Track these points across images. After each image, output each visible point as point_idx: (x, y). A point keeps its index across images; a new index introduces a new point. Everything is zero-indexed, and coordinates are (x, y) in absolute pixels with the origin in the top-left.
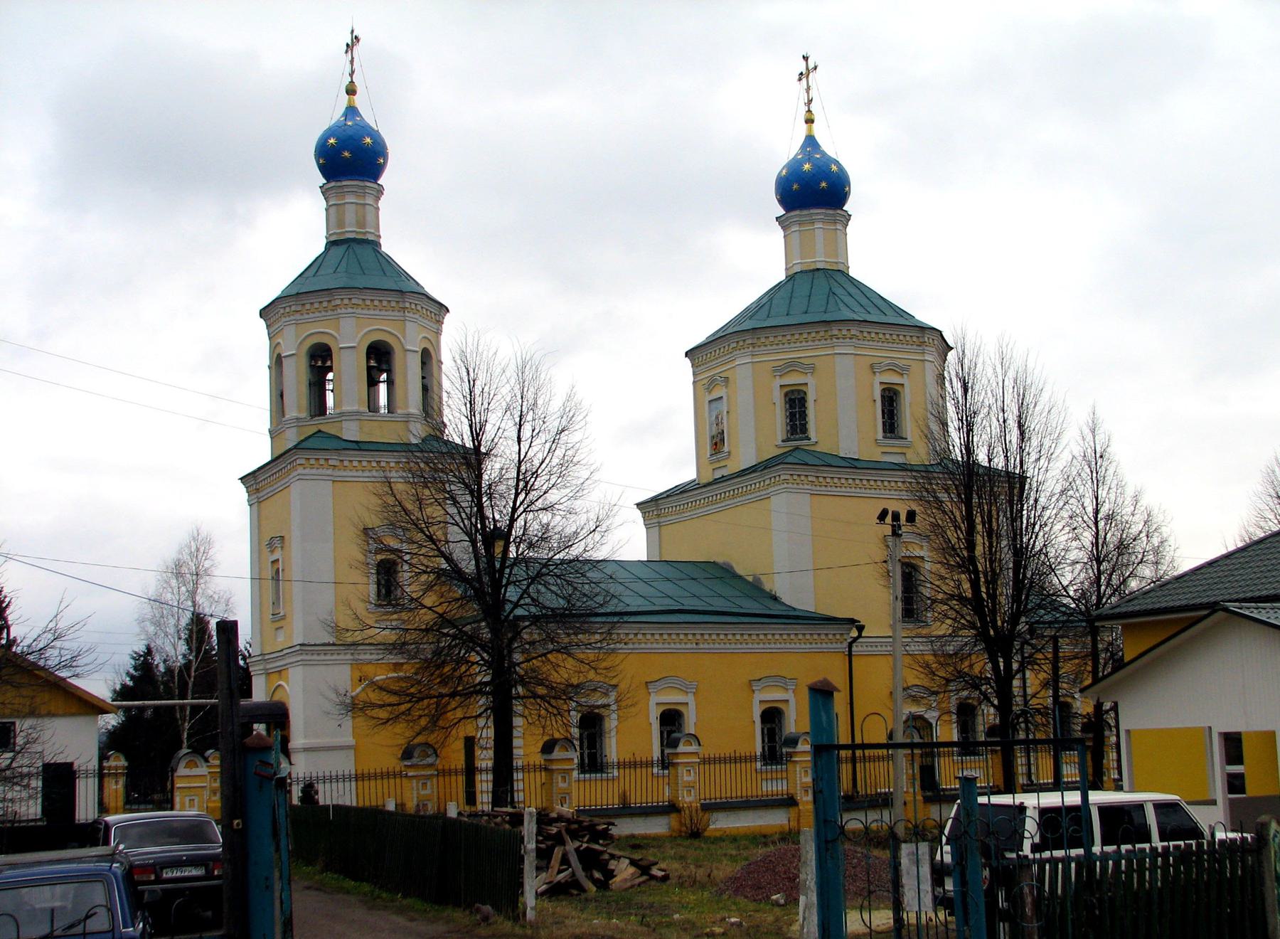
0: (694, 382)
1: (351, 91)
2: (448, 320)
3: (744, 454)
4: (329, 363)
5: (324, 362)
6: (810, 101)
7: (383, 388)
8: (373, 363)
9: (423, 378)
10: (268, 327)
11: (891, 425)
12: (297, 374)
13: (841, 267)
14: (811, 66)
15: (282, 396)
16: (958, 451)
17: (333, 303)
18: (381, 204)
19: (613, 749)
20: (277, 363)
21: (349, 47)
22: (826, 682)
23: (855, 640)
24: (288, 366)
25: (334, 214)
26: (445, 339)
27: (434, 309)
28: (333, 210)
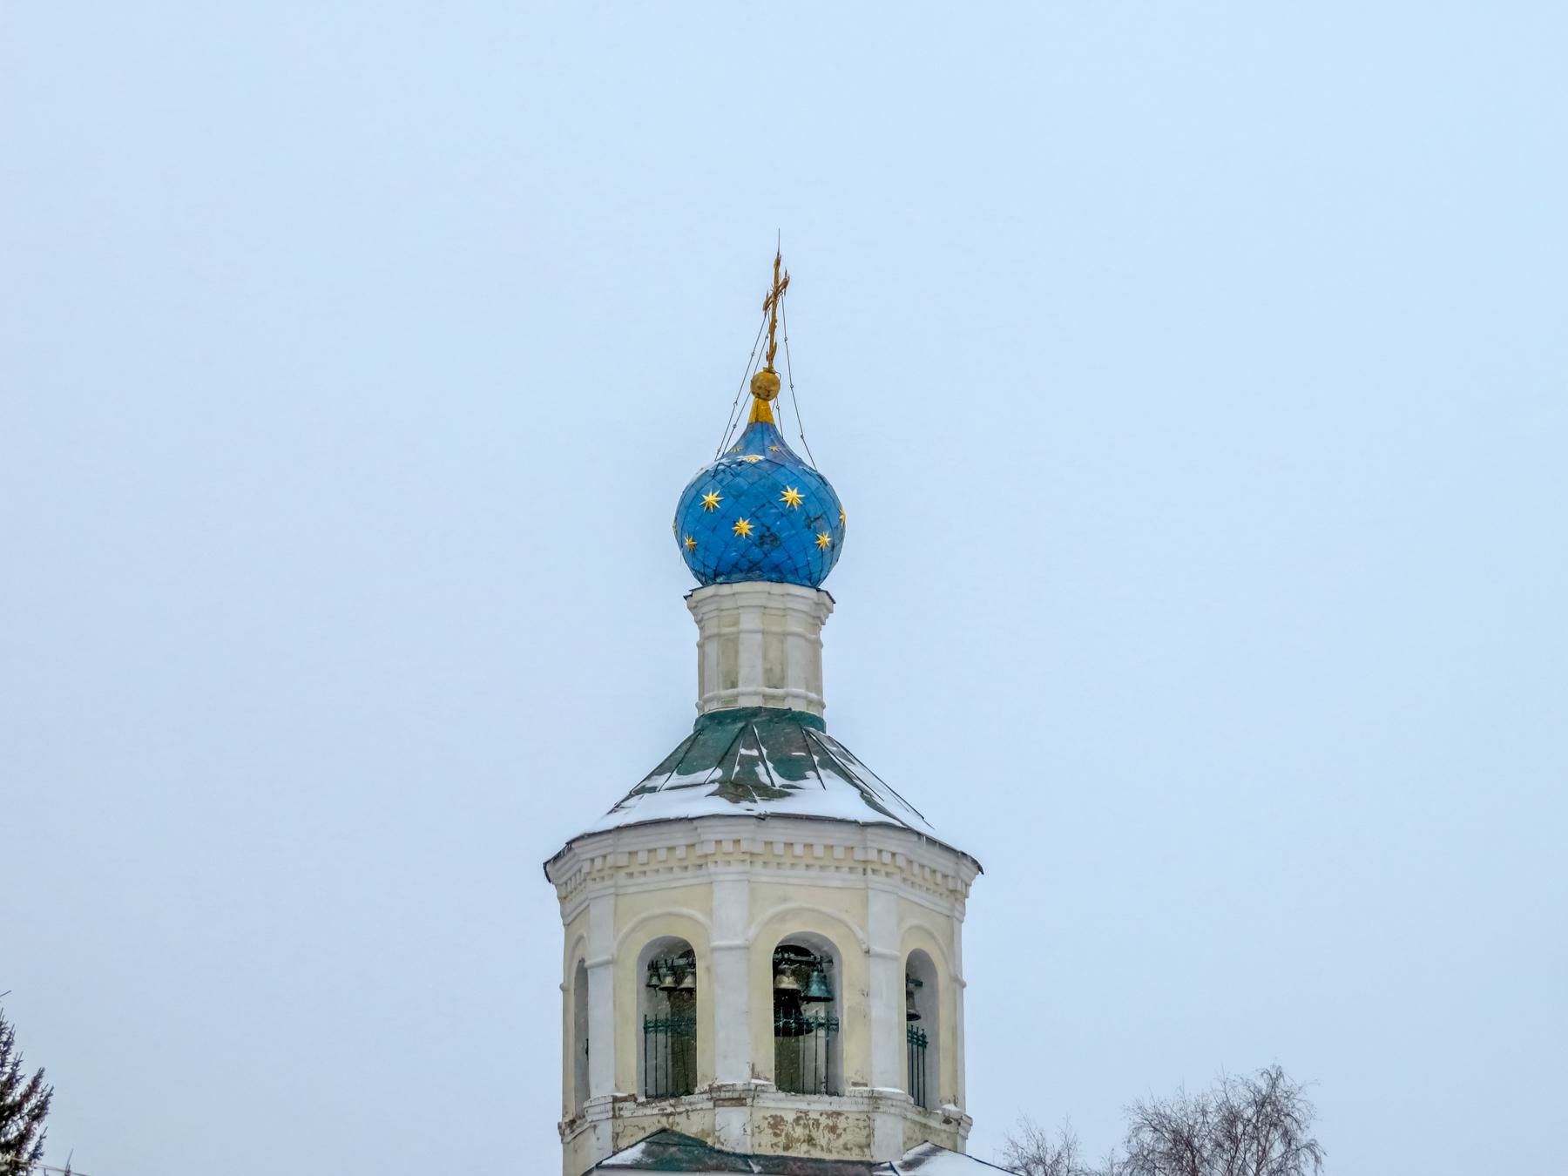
1: (765, 388)
2: (979, 887)
4: (688, 982)
9: (911, 1017)
10: (563, 899)
12: (621, 1007)
16: (772, 1104)
17: (699, 851)
18: (825, 634)
20: (579, 980)
21: (771, 303)
22: (822, 509)
25: (718, 648)
26: (970, 932)
27: (943, 862)
28: (712, 649)
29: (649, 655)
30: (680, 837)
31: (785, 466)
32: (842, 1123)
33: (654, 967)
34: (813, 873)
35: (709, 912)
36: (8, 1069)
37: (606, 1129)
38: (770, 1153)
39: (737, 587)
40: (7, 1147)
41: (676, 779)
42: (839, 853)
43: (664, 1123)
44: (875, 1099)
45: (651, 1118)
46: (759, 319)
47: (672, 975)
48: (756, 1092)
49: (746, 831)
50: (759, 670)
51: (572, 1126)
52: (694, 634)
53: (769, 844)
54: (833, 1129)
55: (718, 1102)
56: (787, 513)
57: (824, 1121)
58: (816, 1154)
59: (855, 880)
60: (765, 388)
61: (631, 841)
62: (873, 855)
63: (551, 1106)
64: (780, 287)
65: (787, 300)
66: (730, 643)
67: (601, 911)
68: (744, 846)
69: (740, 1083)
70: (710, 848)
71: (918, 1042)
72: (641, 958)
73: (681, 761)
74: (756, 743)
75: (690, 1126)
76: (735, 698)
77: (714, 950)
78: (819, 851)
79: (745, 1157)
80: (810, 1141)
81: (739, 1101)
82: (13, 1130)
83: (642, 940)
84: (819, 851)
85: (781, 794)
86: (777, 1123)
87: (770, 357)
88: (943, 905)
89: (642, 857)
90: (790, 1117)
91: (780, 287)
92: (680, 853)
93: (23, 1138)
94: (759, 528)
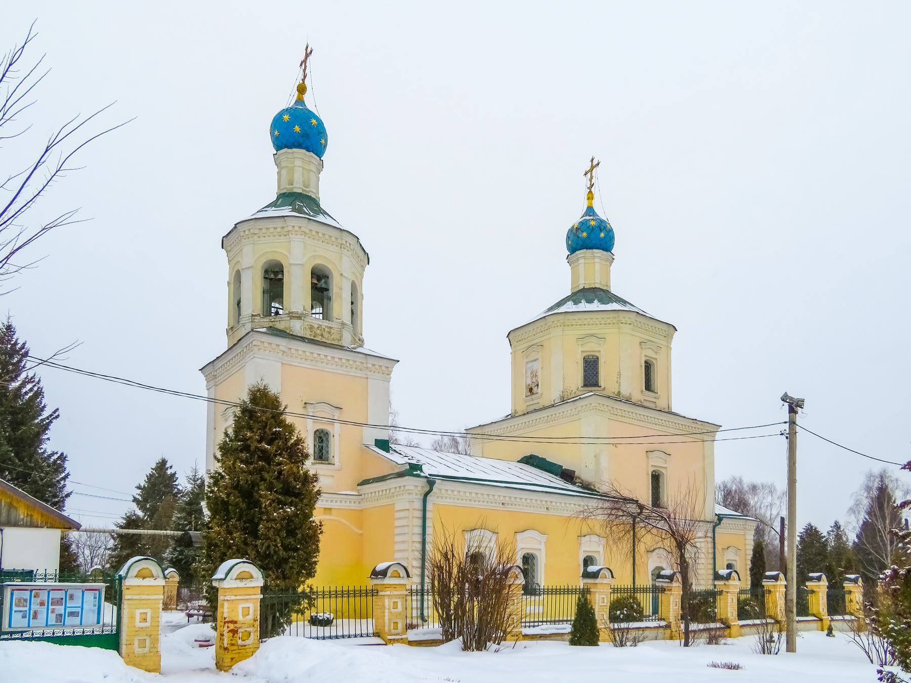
1: (302, 89)
3: (550, 392)
4: (280, 276)
9: (352, 303)
11: (648, 386)
14: (595, 162)
17: (286, 229)
19: (542, 579)
20: (237, 279)
28: (284, 172)
29: (258, 177)
31: (311, 115)
32: (332, 331)
33: (266, 272)
34: (324, 244)
39: (294, 150)
43: (271, 324)
44: (343, 324)
47: (274, 280)
48: (305, 315)
51: (231, 330)
53: (311, 230)
54: (329, 333)
55: (291, 318)
56: (311, 127)
57: (327, 330)
58: (324, 340)
59: (338, 249)
60: (302, 89)
61: (261, 224)
63: (223, 322)
66: (291, 171)
69: (300, 312)
70: (290, 228)
75: (281, 326)
77: (290, 264)
80: (322, 335)
81: (299, 318)
83: (263, 260)
86: (311, 328)
88: (360, 269)
89: (264, 231)
90: (316, 326)
92: (279, 230)
94: (299, 133)
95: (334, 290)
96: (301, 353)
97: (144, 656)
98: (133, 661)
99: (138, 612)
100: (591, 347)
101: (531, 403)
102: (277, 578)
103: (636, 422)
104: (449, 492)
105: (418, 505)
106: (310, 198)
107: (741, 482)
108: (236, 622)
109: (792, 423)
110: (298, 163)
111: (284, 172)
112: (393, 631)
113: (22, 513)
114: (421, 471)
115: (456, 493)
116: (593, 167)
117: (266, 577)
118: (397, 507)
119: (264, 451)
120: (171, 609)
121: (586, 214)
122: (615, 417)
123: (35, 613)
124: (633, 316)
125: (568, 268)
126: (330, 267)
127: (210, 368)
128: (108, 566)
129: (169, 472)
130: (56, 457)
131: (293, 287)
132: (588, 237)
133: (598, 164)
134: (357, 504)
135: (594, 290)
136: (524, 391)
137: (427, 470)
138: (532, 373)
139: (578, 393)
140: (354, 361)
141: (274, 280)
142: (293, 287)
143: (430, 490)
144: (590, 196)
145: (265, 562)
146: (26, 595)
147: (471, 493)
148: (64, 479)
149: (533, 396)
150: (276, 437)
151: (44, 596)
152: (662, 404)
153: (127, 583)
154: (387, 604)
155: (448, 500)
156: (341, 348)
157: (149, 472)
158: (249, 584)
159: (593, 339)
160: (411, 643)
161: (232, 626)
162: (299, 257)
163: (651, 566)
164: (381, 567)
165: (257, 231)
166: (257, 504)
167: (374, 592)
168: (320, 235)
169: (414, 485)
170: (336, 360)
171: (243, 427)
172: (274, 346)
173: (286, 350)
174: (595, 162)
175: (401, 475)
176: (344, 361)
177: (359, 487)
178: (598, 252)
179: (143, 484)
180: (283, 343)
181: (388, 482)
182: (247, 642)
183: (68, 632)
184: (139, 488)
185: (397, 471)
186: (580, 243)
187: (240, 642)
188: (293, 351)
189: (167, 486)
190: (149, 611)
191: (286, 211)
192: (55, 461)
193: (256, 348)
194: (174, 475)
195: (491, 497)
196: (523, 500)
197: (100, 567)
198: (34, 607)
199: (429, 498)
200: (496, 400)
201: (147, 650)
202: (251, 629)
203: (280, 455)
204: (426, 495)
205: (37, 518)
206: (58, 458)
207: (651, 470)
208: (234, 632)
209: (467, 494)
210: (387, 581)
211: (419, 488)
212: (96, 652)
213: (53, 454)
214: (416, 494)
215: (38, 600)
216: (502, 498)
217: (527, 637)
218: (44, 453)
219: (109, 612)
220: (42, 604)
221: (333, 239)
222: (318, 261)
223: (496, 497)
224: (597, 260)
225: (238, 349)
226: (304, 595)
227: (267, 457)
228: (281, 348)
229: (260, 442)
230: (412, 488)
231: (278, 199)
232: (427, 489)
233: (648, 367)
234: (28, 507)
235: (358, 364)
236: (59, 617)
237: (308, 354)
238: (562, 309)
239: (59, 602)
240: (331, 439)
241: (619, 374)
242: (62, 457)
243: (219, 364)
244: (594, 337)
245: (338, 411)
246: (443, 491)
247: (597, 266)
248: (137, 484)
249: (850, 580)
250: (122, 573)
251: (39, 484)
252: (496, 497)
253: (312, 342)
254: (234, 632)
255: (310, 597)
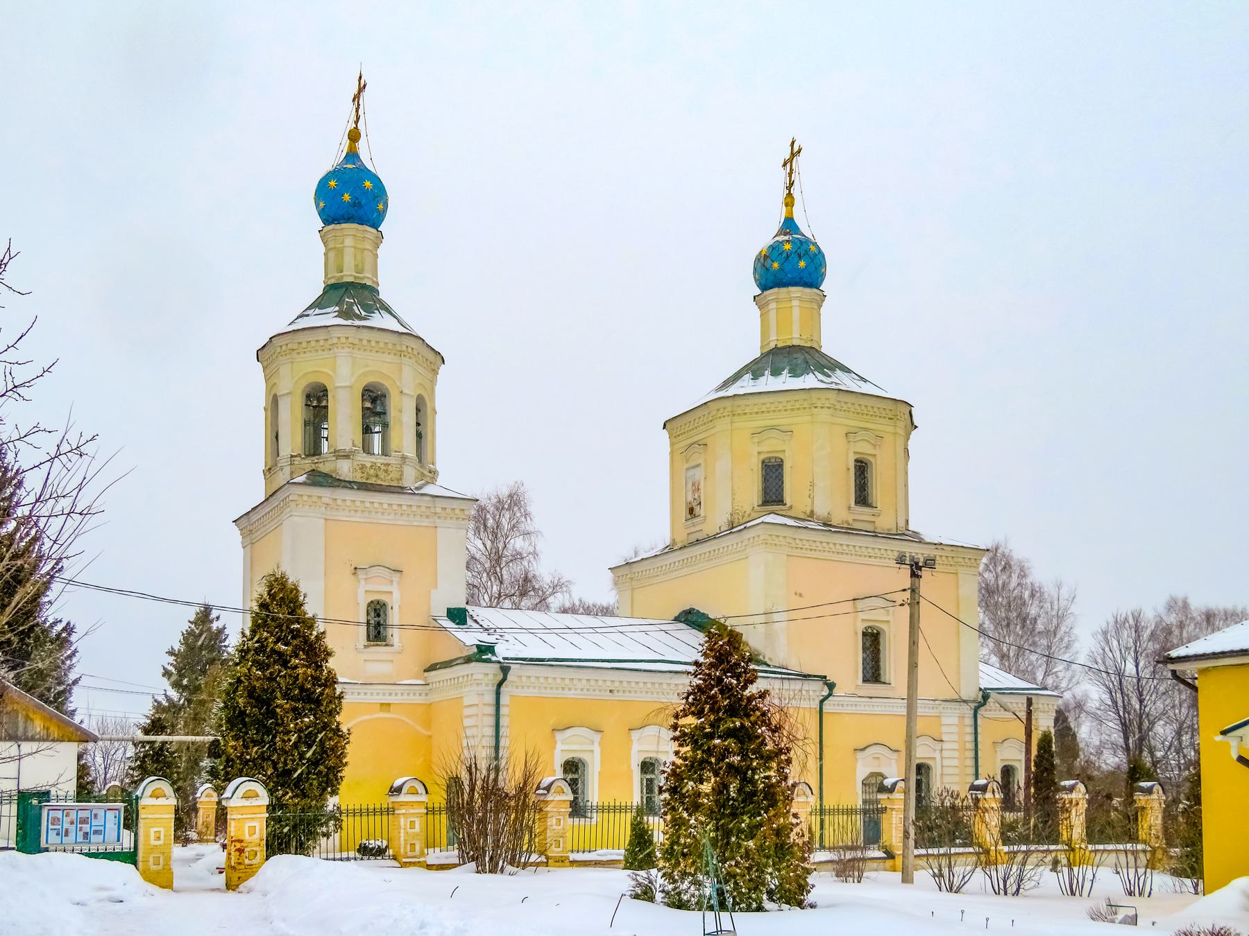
0: (672, 453)
1: (354, 136)
3: (715, 517)
4: (324, 404)
5: (319, 401)
6: (792, 184)
7: (377, 439)
8: (368, 405)
9: (418, 424)
10: (265, 368)
11: (862, 497)
13: (815, 346)
14: (796, 149)
15: (277, 437)
17: (330, 342)
19: (594, 794)
20: (274, 404)
21: (356, 98)
23: (826, 698)
24: (284, 406)
25: (333, 253)
26: (438, 388)
27: (431, 356)
28: (331, 254)
29: (299, 260)
30: (321, 335)
31: (364, 173)
32: (390, 468)
33: (308, 397)
35: (334, 371)
36: (12, 525)
37: (287, 470)
38: (359, 480)
39: (344, 226)
40: (3, 499)
41: (317, 311)
42: (390, 346)
43: (314, 467)
44: (404, 458)
45: (308, 464)
46: (351, 107)
47: (317, 402)
49: (351, 333)
50: (353, 263)
51: (269, 471)
52: (323, 249)
54: (386, 471)
55: (338, 457)
56: (365, 192)
58: (379, 482)
60: (354, 136)
62: (404, 348)
63: (258, 460)
64: (362, 89)
65: (366, 95)
66: (340, 252)
67: (285, 371)
68: (350, 340)
70: (335, 341)
71: (419, 436)
72: (308, 386)
73: (319, 304)
74: (350, 295)
75: (325, 468)
76: (342, 277)
78: (382, 345)
79: (350, 482)
81: (347, 457)
82: (9, 491)
83: (304, 383)
84: (382, 345)
85: (365, 319)
86: (363, 467)
87: (356, 122)
88: (430, 375)
90: (368, 465)
91: (362, 89)
92: (322, 343)
93: (13, 494)
95: (393, 414)
96: (348, 503)
97: (158, 872)
98: (150, 877)
99: (153, 830)
100: (772, 446)
101: (693, 530)
102: (296, 796)
103: (836, 557)
104: (533, 679)
105: (490, 698)
106: (364, 286)
107: (1185, 606)
108: (240, 841)
109: (913, 590)
110: (349, 242)
111: (331, 254)
112: (410, 854)
113: (38, 726)
114: (493, 653)
115: (542, 680)
116: (791, 160)
117: (271, 792)
118: (466, 702)
119: (280, 654)
120: (207, 841)
121: (782, 231)
122: (798, 552)
123: (67, 831)
124: (832, 395)
125: (757, 312)
126: (387, 383)
127: (244, 522)
128: (127, 781)
129: (215, 626)
130: (59, 627)
131: (344, 416)
132: (781, 269)
133: (799, 151)
134: (423, 697)
135: (791, 350)
136: (683, 512)
137: (502, 651)
138: (693, 484)
139: (754, 515)
140: (419, 507)
141: (317, 402)
142: (344, 416)
143: (504, 680)
144: (789, 201)
145: (280, 780)
146: (59, 814)
147: (563, 679)
148: (70, 657)
149: (695, 520)
150: (296, 634)
151: (73, 815)
152: (885, 522)
153: (142, 802)
154: (402, 823)
155: (531, 690)
156: (400, 490)
157: (185, 627)
158: (254, 802)
159: (774, 433)
160: (429, 867)
161: (238, 845)
162: (345, 381)
163: (862, 772)
164: (398, 783)
165: (295, 346)
166: (273, 714)
167: (390, 811)
168: (373, 344)
169: (484, 674)
170: (395, 507)
171: (259, 626)
172: (315, 499)
173: (331, 502)
174: (796, 149)
175: (468, 660)
176: (404, 508)
177: (426, 674)
178: (796, 291)
179: (177, 647)
180: (325, 494)
181: (455, 668)
182: (254, 862)
183: (93, 849)
184: (171, 653)
185: (465, 654)
186: (771, 278)
187: (247, 861)
188: (339, 502)
189: (211, 649)
190: (162, 829)
191: (329, 318)
192: (58, 635)
193: (293, 504)
194: (221, 631)
195: (593, 683)
196: (641, 685)
197: (117, 783)
198: (66, 826)
199: (503, 689)
200: (654, 527)
201: (160, 867)
202: (257, 849)
203: (297, 656)
204: (500, 685)
205: (55, 732)
206: (64, 629)
207: (861, 627)
208: (241, 851)
209: (559, 681)
210: (403, 798)
211: (491, 677)
212: (117, 864)
213: (56, 623)
214: (487, 685)
215: (68, 819)
216: (608, 683)
217: (574, 863)
218: (45, 622)
219: (127, 836)
220: (72, 823)
221: (390, 346)
222: (371, 379)
223: (600, 683)
224: (795, 303)
225: (274, 502)
226: (333, 817)
227: (283, 660)
228: (324, 500)
229: (275, 643)
230: (481, 676)
231: (325, 292)
232: (501, 677)
233: (862, 469)
234: (44, 719)
235: (423, 509)
236: (86, 835)
237: (358, 504)
238: (731, 391)
239: (84, 821)
240: (389, 612)
241: (812, 485)
242: (69, 629)
243: (254, 517)
244: (795, 422)
245: (398, 574)
246: (524, 679)
247: (796, 313)
248: (168, 648)
249: (1143, 790)
250: (139, 793)
251: (51, 691)
252: (600, 683)
253: (364, 487)
254: (241, 851)
255: (336, 817)
